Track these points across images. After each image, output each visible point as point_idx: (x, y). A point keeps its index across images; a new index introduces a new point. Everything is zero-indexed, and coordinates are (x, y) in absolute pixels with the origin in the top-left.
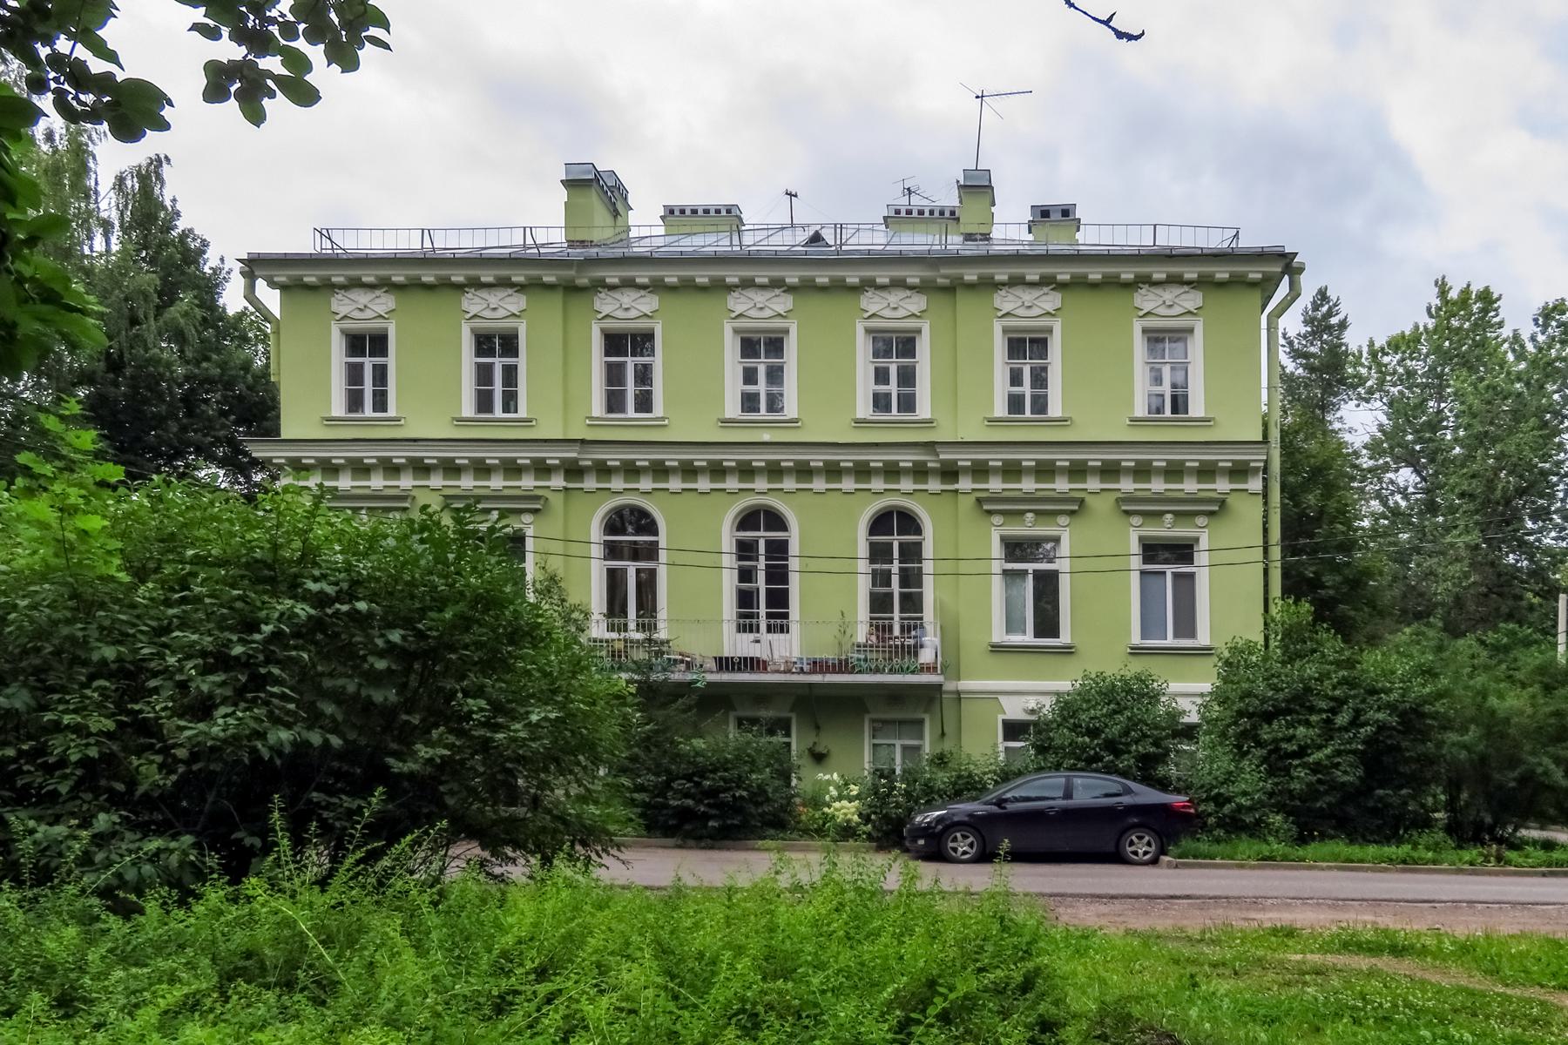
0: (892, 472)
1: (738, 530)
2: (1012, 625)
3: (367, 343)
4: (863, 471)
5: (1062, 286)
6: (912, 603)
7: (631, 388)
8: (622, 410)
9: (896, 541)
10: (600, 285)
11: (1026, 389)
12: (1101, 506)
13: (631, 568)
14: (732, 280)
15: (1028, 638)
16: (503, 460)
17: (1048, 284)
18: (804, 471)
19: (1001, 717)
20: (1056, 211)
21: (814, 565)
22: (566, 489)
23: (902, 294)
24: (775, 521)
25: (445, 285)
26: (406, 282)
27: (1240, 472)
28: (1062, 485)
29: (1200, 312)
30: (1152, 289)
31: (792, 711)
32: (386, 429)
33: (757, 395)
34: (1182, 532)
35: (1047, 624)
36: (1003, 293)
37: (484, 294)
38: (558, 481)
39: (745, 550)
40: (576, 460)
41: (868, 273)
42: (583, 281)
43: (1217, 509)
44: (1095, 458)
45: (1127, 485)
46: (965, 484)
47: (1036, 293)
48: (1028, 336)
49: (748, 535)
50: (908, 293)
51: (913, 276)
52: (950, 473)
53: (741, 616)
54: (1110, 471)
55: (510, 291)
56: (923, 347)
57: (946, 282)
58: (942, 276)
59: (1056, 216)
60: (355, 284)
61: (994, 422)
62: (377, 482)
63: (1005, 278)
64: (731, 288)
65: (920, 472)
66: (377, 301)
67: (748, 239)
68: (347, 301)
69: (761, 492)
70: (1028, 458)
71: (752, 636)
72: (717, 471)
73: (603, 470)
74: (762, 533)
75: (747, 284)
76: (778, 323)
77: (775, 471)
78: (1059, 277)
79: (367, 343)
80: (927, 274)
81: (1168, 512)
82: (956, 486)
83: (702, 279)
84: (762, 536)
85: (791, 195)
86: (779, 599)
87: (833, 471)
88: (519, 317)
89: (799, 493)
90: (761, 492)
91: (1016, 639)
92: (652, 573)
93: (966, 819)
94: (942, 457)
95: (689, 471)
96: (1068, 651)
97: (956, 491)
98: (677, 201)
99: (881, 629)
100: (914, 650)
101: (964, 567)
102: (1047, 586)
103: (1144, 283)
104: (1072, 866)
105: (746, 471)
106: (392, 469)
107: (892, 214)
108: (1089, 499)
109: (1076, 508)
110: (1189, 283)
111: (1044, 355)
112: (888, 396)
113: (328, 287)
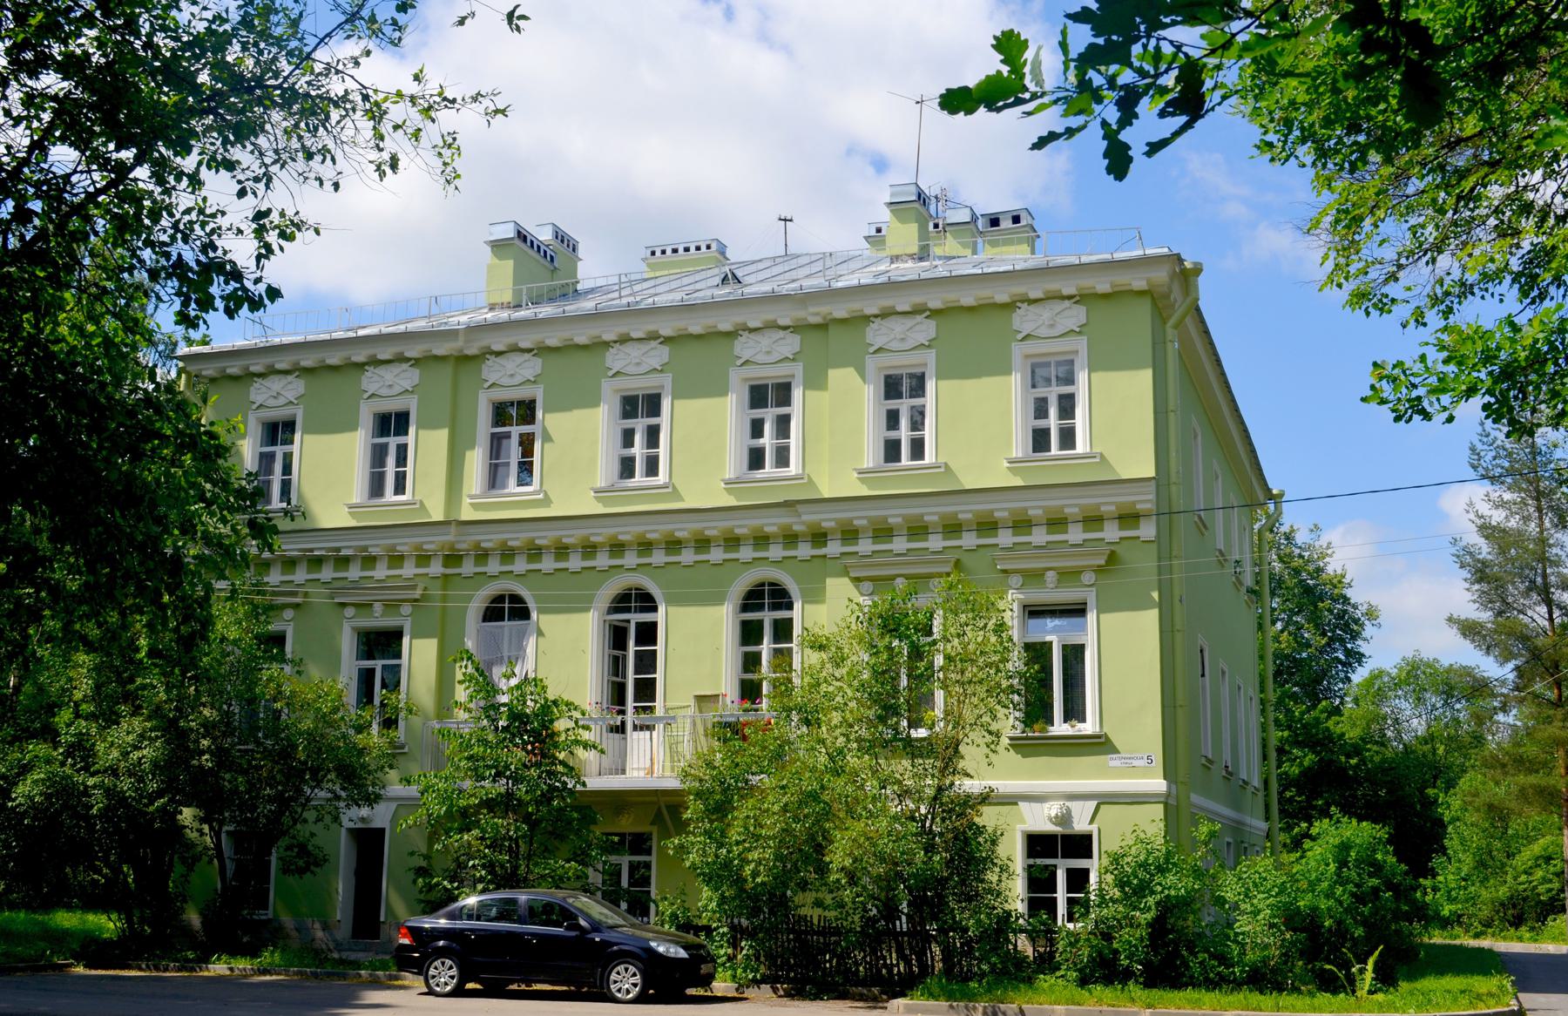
7: (390, 469)
8: (898, 459)
9: (767, 617)
14: (608, 337)
16: (943, 516)
17: (656, 338)
20: (1005, 219)
22: (446, 576)
26: (974, 304)
29: (1084, 329)
30: (751, 336)
31: (651, 824)
37: (381, 370)
38: (969, 540)
41: (1019, 289)
42: (472, 351)
48: (1053, 359)
55: (405, 366)
58: (813, 314)
59: (1006, 223)
60: (272, 372)
66: (290, 387)
68: (264, 389)
73: (482, 556)
79: (640, 405)
81: (1016, 571)
83: (233, 370)
85: (785, 220)
86: (646, 690)
88: (661, 371)
93: (637, 950)
94: (805, 518)
97: (825, 556)
98: (658, 241)
103: (1022, 302)
104: (494, 1000)
107: (873, 233)
108: (967, 560)
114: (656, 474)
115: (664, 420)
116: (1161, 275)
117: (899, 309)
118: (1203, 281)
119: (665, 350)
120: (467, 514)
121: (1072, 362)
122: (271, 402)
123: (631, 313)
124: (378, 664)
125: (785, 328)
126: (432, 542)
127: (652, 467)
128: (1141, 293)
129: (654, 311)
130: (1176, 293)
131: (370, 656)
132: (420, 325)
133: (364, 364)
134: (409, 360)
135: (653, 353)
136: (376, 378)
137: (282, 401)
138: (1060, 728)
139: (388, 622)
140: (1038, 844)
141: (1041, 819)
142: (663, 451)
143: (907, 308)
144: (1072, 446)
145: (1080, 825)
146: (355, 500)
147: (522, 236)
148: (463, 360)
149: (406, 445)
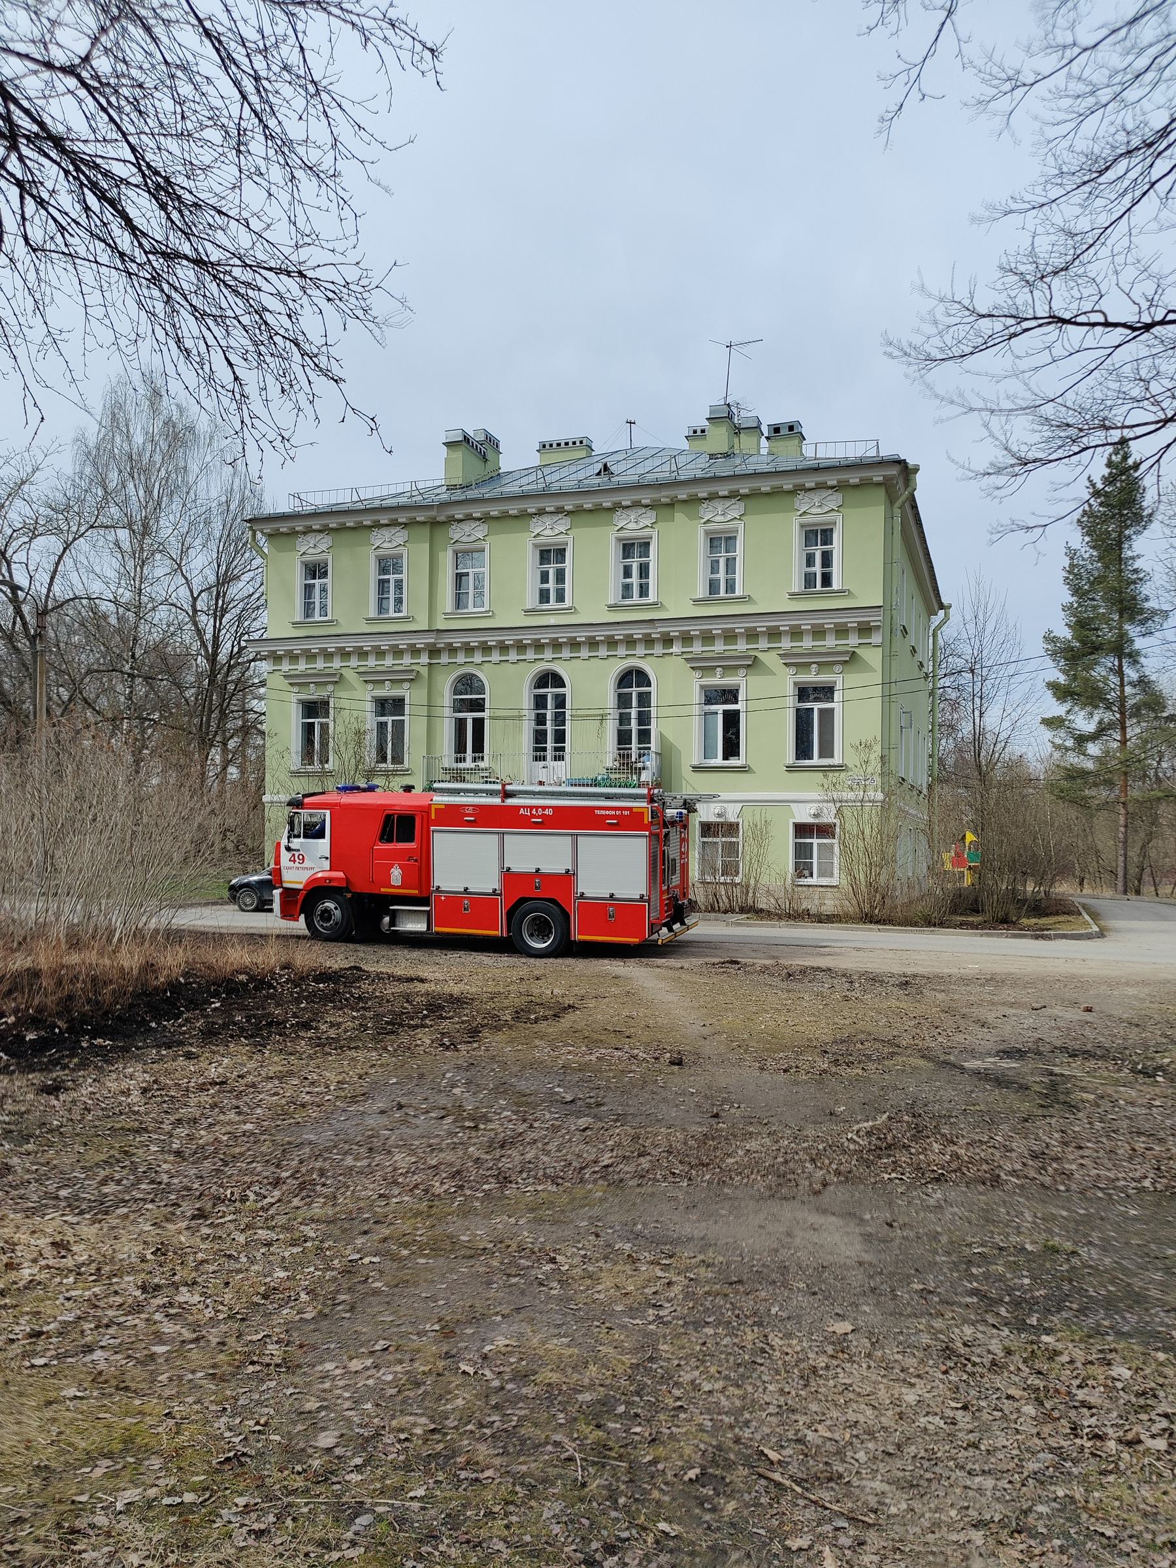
0: (630, 642)
1: (619, 687)
2: (708, 753)
3: (550, 554)
4: (612, 643)
5: (744, 497)
6: (644, 736)
9: (634, 691)
10: (452, 520)
11: (551, 585)
12: (771, 659)
13: (470, 716)
15: (719, 761)
16: (588, 638)
17: (735, 497)
18: (574, 645)
19: (791, 821)
21: (515, 713)
23: (474, 524)
24: (558, 681)
25: (359, 527)
27: (865, 630)
28: (742, 646)
32: (472, 621)
33: (548, 590)
34: (824, 678)
35: (731, 748)
36: (704, 506)
39: (540, 702)
40: (435, 644)
42: (442, 518)
43: (851, 660)
44: (761, 625)
45: (286, 666)
46: (676, 649)
47: (728, 503)
48: (819, 528)
49: (542, 691)
50: (644, 510)
51: (646, 498)
52: (668, 641)
53: (536, 749)
54: (774, 634)
55: (398, 528)
56: (836, 537)
57: (667, 500)
58: (664, 496)
61: (697, 602)
62: (320, 664)
63: (705, 495)
64: (532, 515)
65: (649, 641)
67: (808, 451)
69: (547, 662)
70: (829, 622)
71: (542, 763)
72: (521, 647)
73: (452, 650)
74: (550, 690)
75: (712, 497)
76: (561, 538)
77: (556, 645)
78: (741, 491)
80: (655, 496)
82: (671, 651)
84: (550, 691)
87: (593, 644)
89: (574, 660)
90: (547, 662)
91: (713, 762)
92: (831, 711)
95: (503, 648)
96: (841, 768)
99: (624, 757)
100: (639, 771)
101: (977, 700)
102: (731, 720)
105: (539, 646)
106: (397, 652)
109: (753, 665)
110: (832, 487)
111: (563, 561)
112: (548, 590)
113: (293, 533)
114: (647, 595)
115: (568, 565)
116: (893, 471)
117: (721, 493)
118: (919, 477)
119: (568, 520)
120: (441, 625)
121: (648, 543)
122: (464, 539)
123: (545, 494)
124: (389, 719)
125: (479, 519)
126: (420, 642)
127: (561, 597)
128: (878, 484)
129: (756, 475)
130: (901, 485)
131: (383, 715)
132: (403, 500)
133: (371, 527)
134: (401, 524)
135: (563, 521)
136: (711, 508)
137: (472, 538)
138: (816, 760)
139: (396, 692)
140: (802, 830)
141: (804, 815)
142: (568, 586)
143: (726, 493)
144: (733, 591)
145: (732, 818)
146: (700, 595)
147: (466, 439)
148: (434, 524)
149: (402, 581)
